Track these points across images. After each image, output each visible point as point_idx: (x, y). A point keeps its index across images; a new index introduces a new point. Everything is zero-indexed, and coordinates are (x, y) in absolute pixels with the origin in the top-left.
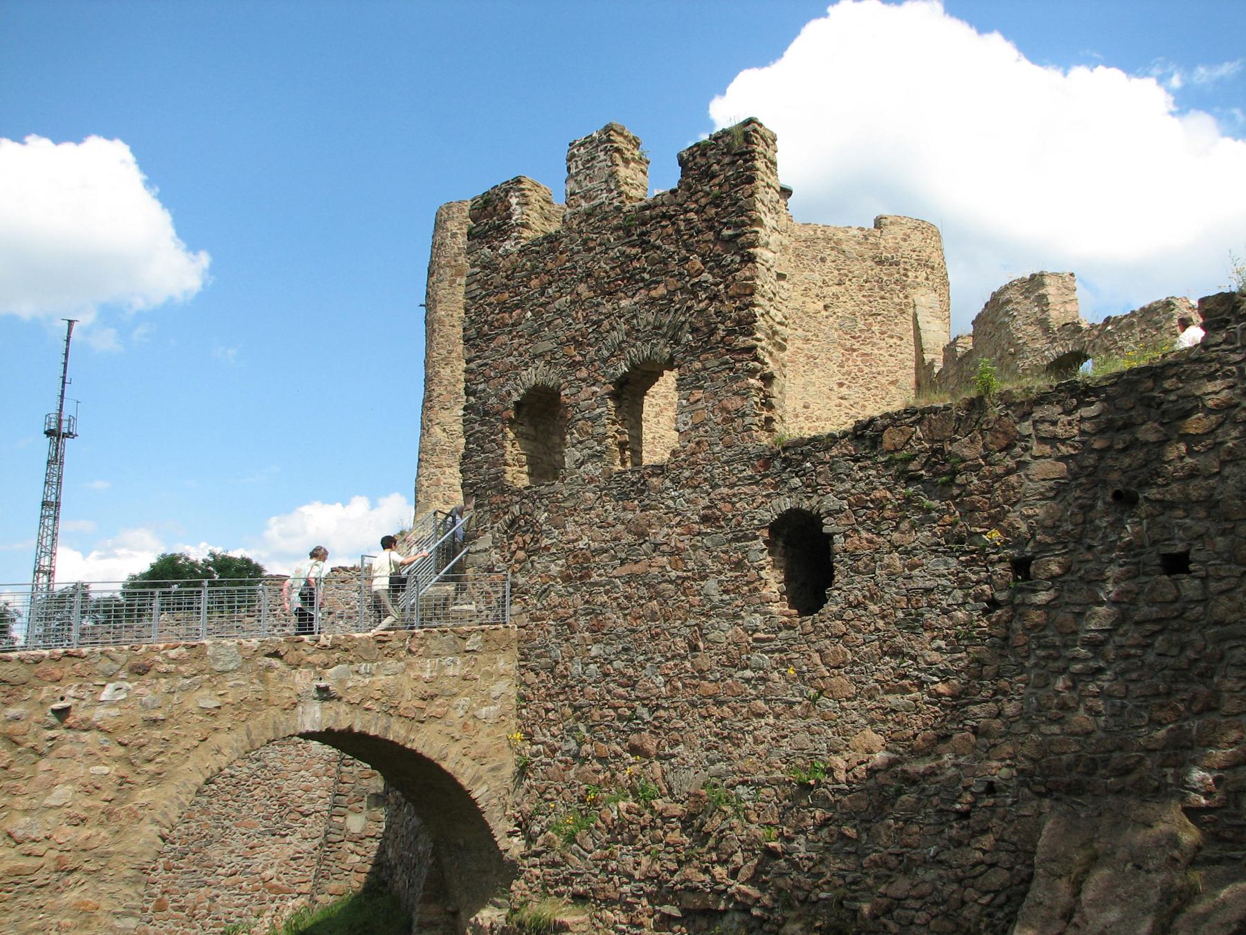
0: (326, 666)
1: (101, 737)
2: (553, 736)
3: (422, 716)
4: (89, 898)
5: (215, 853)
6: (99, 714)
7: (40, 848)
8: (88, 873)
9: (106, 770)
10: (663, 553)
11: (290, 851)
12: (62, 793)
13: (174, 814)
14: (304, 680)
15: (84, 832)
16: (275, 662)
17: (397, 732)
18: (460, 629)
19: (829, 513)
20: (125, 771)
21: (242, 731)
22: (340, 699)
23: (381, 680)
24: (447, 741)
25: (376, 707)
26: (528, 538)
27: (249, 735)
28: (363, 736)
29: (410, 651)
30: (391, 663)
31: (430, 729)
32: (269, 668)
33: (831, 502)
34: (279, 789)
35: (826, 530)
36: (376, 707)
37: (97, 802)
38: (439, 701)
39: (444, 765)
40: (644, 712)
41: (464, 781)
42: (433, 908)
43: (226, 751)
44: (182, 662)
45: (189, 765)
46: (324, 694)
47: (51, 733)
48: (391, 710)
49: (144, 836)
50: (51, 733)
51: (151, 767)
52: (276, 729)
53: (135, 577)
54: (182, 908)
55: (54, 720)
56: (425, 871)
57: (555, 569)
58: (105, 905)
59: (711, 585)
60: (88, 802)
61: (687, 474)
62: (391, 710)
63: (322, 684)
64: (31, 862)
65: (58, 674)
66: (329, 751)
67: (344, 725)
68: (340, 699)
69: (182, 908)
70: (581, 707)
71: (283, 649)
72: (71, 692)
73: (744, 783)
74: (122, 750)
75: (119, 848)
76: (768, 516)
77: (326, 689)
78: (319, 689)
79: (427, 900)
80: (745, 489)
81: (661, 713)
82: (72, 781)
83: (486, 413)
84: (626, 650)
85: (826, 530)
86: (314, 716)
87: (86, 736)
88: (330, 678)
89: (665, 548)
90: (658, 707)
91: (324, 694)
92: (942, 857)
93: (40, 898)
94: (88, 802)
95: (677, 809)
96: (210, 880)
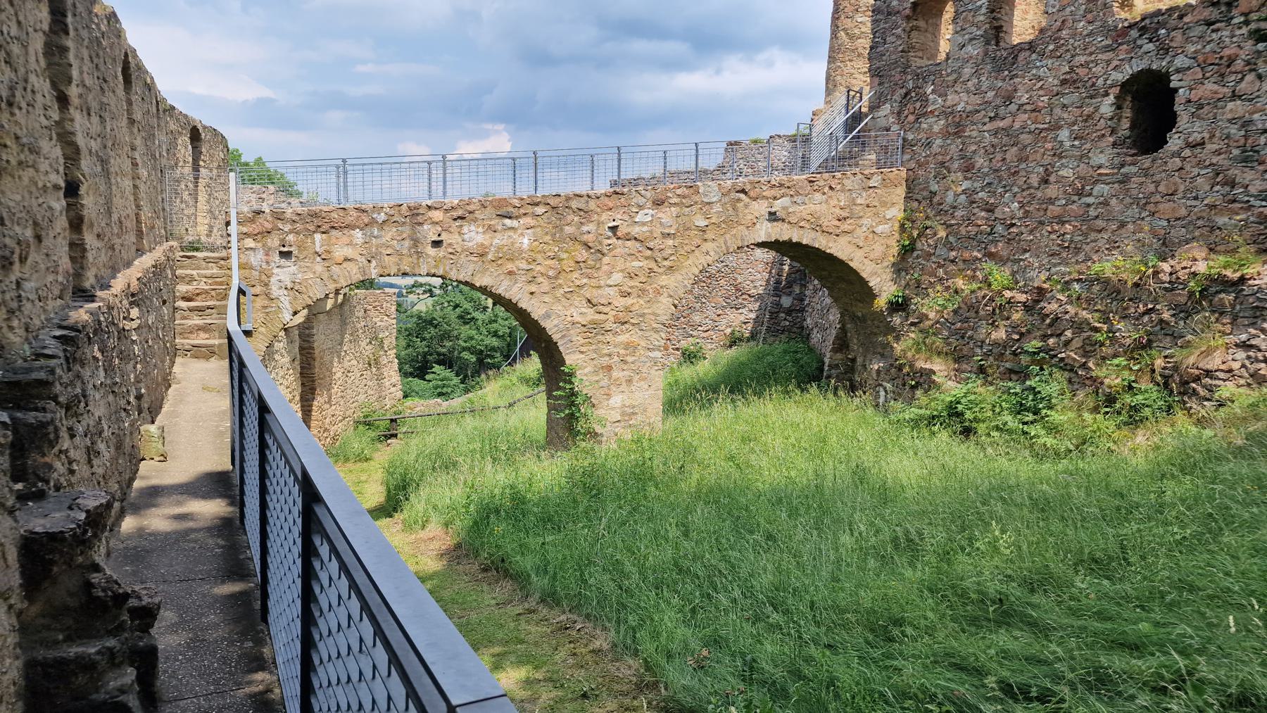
0: (775, 198)
1: (638, 245)
2: (929, 245)
3: (838, 231)
4: (635, 339)
5: (697, 318)
6: (636, 230)
7: (605, 309)
8: (633, 324)
9: (641, 264)
10: (1025, 112)
11: (742, 318)
12: (617, 278)
13: (681, 292)
14: (761, 208)
15: (629, 301)
16: (742, 196)
17: (821, 242)
18: (866, 172)
19: (1178, 71)
20: (653, 265)
21: (721, 240)
22: (783, 220)
23: (811, 207)
24: (854, 248)
25: (807, 226)
26: (918, 105)
27: (725, 243)
28: (799, 244)
29: (831, 188)
30: (818, 196)
31: (843, 240)
32: (739, 200)
33: (1180, 61)
34: (735, 280)
35: (1172, 85)
36: (807, 226)
37: (635, 283)
38: (849, 221)
39: (851, 264)
40: (999, 228)
41: (864, 275)
42: (839, 356)
43: (712, 253)
44: (684, 197)
45: (689, 262)
46: (773, 217)
47: (609, 242)
48: (818, 228)
49: (664, 307)
50: (609, 242)
51: (666, 263)
52: (742, 240)
53: (135, 56)
54: (677, 349)
55: (610, 234)
56: (834, 332)
57: (936, 128)
58: (643, 344)
59: (1064, 134)
60: (632, 283)
61: (1051, 47)
62: (818, 228)
63: (773, 210)
64: (602, 317)
65: (611, 205)
66: (769, 255)
67: (785, 238)
68: (783, 220)
69: (677, 349)
70: (952, 225)
71: (747, 188)
72: (619, 216)
73: (1079, 281)
74: (649, 252)
75: (649, 311)
76: (1120, 77)
77: (775, 213)
78: (770, 213)
79: (835, 350)
80: (1100, 56)
81: (1014, 230)
82: (622, 271)
83: (889, 14)
84: (989, 184)
85: (1172, 85)
86: (766, 231)
87: (629, 243)
88: (778, 206)
89: (1028, 107)
90: (1013, 225)
91: (773, 217)
92: (1253, 342)
93: (609, 337)
94: (632, 283)
95: (1022, 298)
96: (694, 333)
